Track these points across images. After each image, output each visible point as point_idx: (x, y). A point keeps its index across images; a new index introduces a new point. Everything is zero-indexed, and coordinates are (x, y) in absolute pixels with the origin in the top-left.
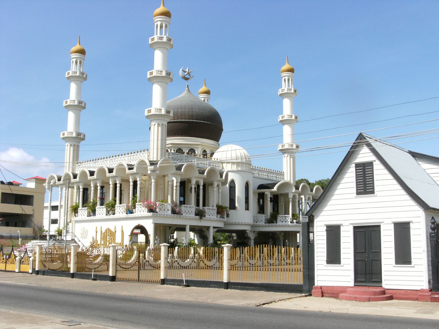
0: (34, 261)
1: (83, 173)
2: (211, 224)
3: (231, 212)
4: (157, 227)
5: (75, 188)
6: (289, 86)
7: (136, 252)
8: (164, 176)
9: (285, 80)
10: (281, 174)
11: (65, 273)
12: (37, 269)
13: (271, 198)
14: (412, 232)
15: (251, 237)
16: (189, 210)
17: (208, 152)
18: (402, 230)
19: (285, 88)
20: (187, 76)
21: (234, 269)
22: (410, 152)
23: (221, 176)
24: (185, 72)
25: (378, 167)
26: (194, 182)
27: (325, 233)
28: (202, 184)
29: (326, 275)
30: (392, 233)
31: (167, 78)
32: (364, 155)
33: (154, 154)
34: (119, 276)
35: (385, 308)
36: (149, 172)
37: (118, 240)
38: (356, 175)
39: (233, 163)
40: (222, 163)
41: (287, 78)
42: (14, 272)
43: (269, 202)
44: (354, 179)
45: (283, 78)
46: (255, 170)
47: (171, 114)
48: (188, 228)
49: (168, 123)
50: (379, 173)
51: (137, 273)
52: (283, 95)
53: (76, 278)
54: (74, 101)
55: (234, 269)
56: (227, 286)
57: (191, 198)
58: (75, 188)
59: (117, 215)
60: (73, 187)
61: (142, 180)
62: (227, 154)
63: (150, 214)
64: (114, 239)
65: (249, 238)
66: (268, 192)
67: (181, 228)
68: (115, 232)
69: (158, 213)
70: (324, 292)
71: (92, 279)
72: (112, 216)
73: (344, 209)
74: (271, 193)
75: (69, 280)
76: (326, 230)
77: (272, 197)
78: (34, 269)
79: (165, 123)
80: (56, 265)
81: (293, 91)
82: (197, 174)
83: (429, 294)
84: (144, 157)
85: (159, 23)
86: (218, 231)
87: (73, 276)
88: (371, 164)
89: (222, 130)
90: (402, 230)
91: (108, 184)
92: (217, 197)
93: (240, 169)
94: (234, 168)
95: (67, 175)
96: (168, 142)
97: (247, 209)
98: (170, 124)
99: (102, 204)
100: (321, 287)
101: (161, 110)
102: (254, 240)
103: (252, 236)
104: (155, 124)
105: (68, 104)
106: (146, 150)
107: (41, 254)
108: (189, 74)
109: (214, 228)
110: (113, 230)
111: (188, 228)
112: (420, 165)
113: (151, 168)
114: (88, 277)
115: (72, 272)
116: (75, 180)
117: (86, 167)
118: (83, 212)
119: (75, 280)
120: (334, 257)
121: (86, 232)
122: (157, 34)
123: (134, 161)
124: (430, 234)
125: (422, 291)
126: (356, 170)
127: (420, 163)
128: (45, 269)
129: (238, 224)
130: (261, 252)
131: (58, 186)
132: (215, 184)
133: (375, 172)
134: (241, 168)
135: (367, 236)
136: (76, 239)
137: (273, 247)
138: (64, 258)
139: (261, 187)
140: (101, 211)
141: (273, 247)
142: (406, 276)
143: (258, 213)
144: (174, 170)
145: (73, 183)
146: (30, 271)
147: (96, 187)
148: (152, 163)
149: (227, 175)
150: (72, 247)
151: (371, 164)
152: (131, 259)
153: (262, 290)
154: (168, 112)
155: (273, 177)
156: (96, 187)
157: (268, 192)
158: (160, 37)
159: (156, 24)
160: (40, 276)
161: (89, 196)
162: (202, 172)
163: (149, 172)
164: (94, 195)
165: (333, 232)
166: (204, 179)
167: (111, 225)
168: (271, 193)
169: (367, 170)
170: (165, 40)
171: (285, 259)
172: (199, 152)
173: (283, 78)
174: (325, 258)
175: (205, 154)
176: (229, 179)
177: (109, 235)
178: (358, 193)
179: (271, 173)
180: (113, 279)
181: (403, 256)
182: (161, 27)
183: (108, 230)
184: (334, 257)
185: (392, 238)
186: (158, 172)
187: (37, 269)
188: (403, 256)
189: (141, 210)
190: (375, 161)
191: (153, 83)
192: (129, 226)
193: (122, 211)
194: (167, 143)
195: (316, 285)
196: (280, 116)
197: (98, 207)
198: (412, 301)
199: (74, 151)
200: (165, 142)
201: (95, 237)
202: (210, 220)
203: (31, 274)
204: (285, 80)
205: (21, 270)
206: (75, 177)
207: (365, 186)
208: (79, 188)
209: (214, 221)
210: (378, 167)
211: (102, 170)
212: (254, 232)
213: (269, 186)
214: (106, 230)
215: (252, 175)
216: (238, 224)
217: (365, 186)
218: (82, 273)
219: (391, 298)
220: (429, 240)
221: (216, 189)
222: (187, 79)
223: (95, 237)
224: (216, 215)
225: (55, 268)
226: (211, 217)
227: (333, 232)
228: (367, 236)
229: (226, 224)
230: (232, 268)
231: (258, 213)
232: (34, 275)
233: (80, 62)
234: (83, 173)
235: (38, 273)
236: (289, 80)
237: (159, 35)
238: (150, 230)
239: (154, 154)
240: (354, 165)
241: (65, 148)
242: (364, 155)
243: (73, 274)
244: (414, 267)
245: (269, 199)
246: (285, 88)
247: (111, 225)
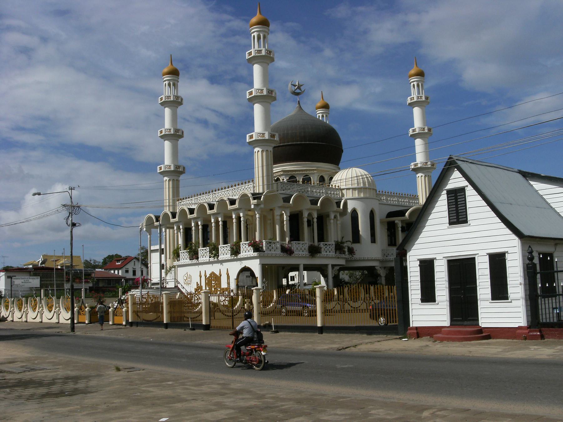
0: (127, 312)
1: (201, 207)
2: (330, 262)
3: (355, 246)
4: (265, 268)
5: (175, 228)
6: (419, 93)
7: (240, 298)
8: (271, 210)
9: (414, 85)
10: (416, 198)
11: (159, 324)
12: (130, 321)
13: (402, 227)
14: (508, 264)
15: (382, 275)
16: (301, 248)
17: (326, 178)
18: (498, 262)
19: (414, 95)
20: (298, 91)
21: (358, 311)
22: (520, 172)
23: (338, 205)
24: (295, 86)
25: (470, 192)
26: (305, 215)
27: (418, 269)
28: (315, 216)
29: (422, 315)
30: (487, 265)
31: (267, 98)
32: (456, 180)
33: (258, 185)
34: (214, 323)
35: (473, 349)
36: (252, 207)
37: (224, 285)
38: (448, 203)
39: (354, 189)
40: (342, 190)
41: (415, 83)
42: (121, 325)
43: (400, 232)
44: (446, 208)
45: (412, 84)
46: (383, 195)
47: (277, 138)
48: (301, 267)
49: (275, 147)
50: (473, 199)
51: (231, 320)
52: (412, 105)
53: (170, 328)
54: (170, 129)
55: (358, 311)
56: (321, 330)
57: (303, 233)
58: (175, 228)
59: (201, 260)
60: (174, 228)
61: (247, 215)
62: (347, 179)
63: (256, 254)
64: (220, 284)
65: (379, 275)
66: (398, 220)
67: (295, 268)
68: (221, 276)
69: (266, 252)
70: (420, 332)
71: (190, 329)
72: (195, 261)
73: (437, 241)
74: (402, 221)
75: (160, 331)
76: (419, 265)
77: (405, 225)
78: (127, 321)
79: (271, 149)
80: (151, 316)
81: (424, 99)
82: (309, 205)
83: (527, 331)
84: (248, 189)
85: (256, 34)
86: (339, 270)
87: (167, 326)
88: (462, 190)
89: (342, 151)
90: (498, 262)
91: (231, 217)
92: (336, 231)
93: (362, 195)
94: (356, 195)
95: (166, 215)
96: (275, 170)
97: (373, 241)
98: (276, 149)
99: (225, 242)
100: (417, 328)
101: (263, 134)
102: (385, 277)
103: (382, 273)
104: (258, 151)
105: (163, 134)
106: (251, 181)
107: (134, 304)
108: (299, 88)
109: (333, 266)
110: (218, 274)
111: (301, 267)
112: (530, 184)
113: (253, 202)
114: (185, 326)
115: (165, 322)
116: (174, 219)
117: (192, 203)
118: (184, 256)
119: (170, 331)
120: (428, 295)
121: (189, 276)
122: (254, 47)
123: (235, 193)
124: (527, 265)
125: (520, 328)
126: (448, 197)
127: (532, 183)
128: (139, 320)
129: (364, 260)
130: (367, 291)
131: (156, 227)
132: (332, 216)
133: (468, 199)
134: (364, 194)
135: (461, 270)
136: (179, 286)
137: (359, 288)
138: (156, 307)
139: (390, 215)
140: (204, 253)
141: (359, 288)
142: (504, 313)
143: (389, 245)
144: (281, 203)
145: (173, 223)
146: (124, 323)
147: (217, 222)
148: (256, 196)
149: (345, 204)
150: (164, 295)
151: (462, 190)
152: (270, 304)
153: (357, 333)
154: (272, 136)
155: (405, 202)
156: (217, 222)
157: (398, 220)
158: (258, 50)
159: (253, 35)
160: (134, 328)
161: (228, 230)
162: (314, 202)
163: (252, 207)
164: (200, 235)
165: (427, 267)
166: (318, 210)
167: (215, 268)
168: (402, 221)
169: (459, 197)
170: (263, 53)
171: (374, 298)
172: (315, 179)
173: (412, 84)
174: (419, 296)
175: (322, 179)
176: (349, 210)
177: (214, 279)
178: (451, 223)
179: (402, 197)
180: (207, 327)
181: (500, 292)
182: (259, 38)
183: (213, 274)
184: (428, 295)
185: (487, 272)
186: (262, 206)
187: (130, 321)
188: (500, 292)
189: (246, 250)
190: (467, 186)
191: (254, 104)
192: (235, 268)
193: (186, 257)
194: (274, 172)
195: (411, 326)
196: (411, 130)
197: (221, 245)
198: (511, 340)
199: (173, 188)
200: (272, 170)
201: (199, 283)
202: (327, 257)
203: (125, 325)
204: (414, 85)
205: (80, 321)
206: (174, 215)
207: (458, 216)
208: (179, 228)
209: (332, 258)
210: (470, 192)
211: (222, 202)
212: (385, 268)
213: (401, 213)
214: (211, 275)
215: (378, 202)
216: (364, 260)
217: (458, 216)
218: (176, 322)
219: (488, 337)
220: (526, 272)
221: (332, 221)
222: (298, 94)
223: (199, 283)
224: (334, 251)
225: (149, 319)
226: (328, 253)
227: (427, 267)
228: (461, 270)
229: (347, 261)
230: (326, 312)
231: (389, 245)
232: (128, 326)
233: (174, 85)
234: (183, 211)
235: (131, 324)
236: (418, 85)
237: (256, 48)
238: (258, 273)
239: (258, 185)
240: (445, 192)
241: (163, 185)
242: (456, 180)
243: (166, 324)
244: (511, 302)
245: (400, 229)
246: (414, 95)
247: (215, 268)
